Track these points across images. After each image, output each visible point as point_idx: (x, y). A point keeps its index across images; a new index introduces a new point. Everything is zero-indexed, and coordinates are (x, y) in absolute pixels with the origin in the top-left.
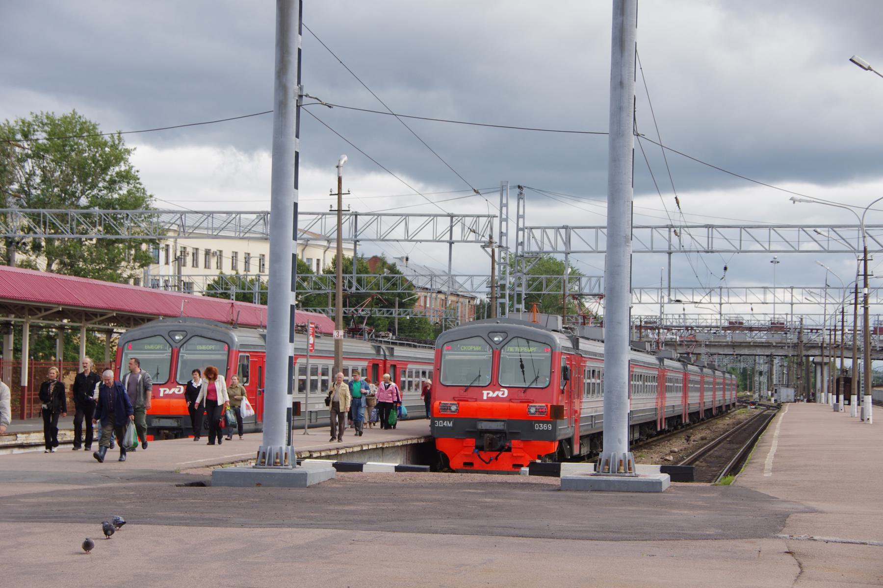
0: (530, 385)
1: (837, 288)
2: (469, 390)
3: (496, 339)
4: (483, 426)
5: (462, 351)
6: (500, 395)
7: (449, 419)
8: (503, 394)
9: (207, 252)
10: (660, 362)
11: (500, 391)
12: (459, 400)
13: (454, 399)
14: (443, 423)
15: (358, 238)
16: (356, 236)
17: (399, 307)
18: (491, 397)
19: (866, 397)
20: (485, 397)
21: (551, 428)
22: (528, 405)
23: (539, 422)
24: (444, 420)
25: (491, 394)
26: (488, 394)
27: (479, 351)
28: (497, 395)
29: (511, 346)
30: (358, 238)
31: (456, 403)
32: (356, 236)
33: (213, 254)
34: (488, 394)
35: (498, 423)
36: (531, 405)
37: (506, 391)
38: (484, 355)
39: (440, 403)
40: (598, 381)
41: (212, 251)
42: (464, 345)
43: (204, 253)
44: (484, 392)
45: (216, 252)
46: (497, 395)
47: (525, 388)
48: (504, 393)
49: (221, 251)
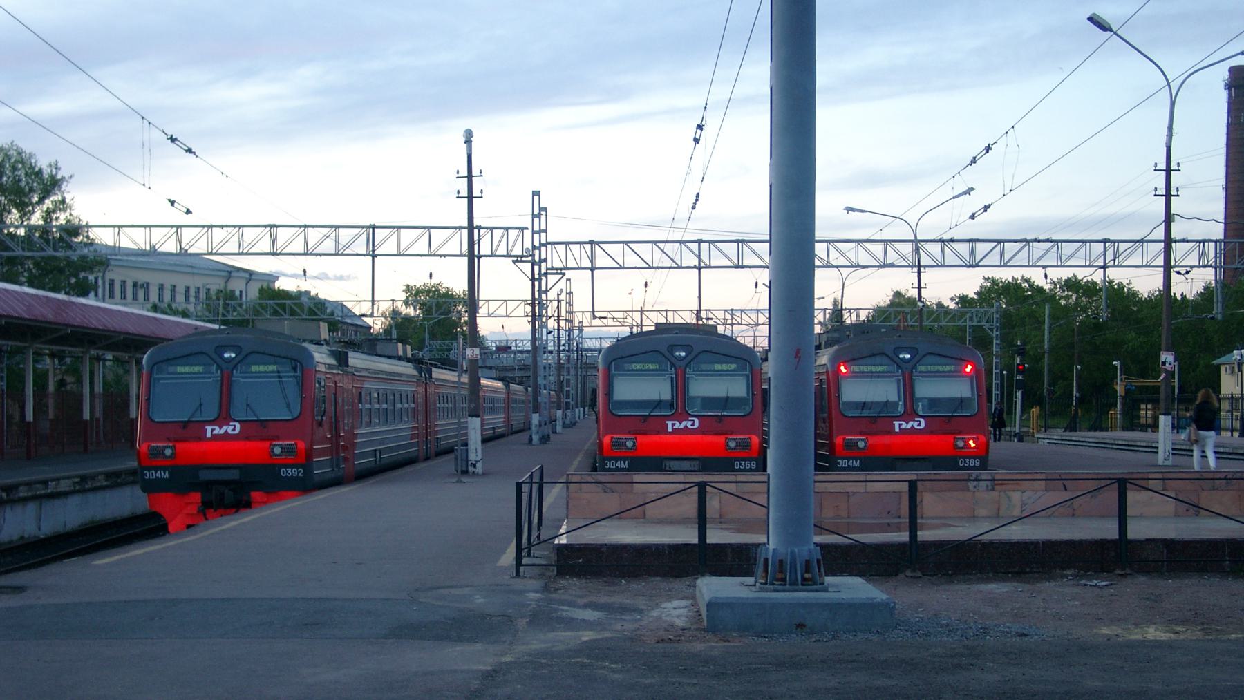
0: (193, 415)
1: (145, 227)
2: (189, 429)
3: (226, 355)
4: (205, 475)
5: (625, 371)
6: (230, 431)
7: (164, 468)
8: (234, 429)
9: (135, 285)
10: (420, 371)
11: (914, 420)
12: (176, 441)
13: (169, 440)
14: (848, 462)
15: (376, 253)
16: (373, 251)
17: (963, 329)
18: (218, 435)
19: (534, 415)
20: (209, 435)
21: (979, 463)
22: (955, 438)
23: (286, 466)
24: (616, 459)
25: (217, 431)
26: (673, 425)
27: (656, 370)
28: (226, 431)
29: (923, 365)
30: (376, 253)
31: (171, 445)
32: (373, 251)
33: (141, 285)
34: (900, 425)
35: (232, 471)
36: (730, 437)
37: (922, 421)
38: (209, 378)
39: (612, 438)
40: (491, 405)
41: (139, 283)
42: (172, 365)
43: (132, 284)
44: (667, 422)
45: (143, 285)
46: (226, 431)
47: (185, 422)
48: (233, 428)
49: (148, 284)
